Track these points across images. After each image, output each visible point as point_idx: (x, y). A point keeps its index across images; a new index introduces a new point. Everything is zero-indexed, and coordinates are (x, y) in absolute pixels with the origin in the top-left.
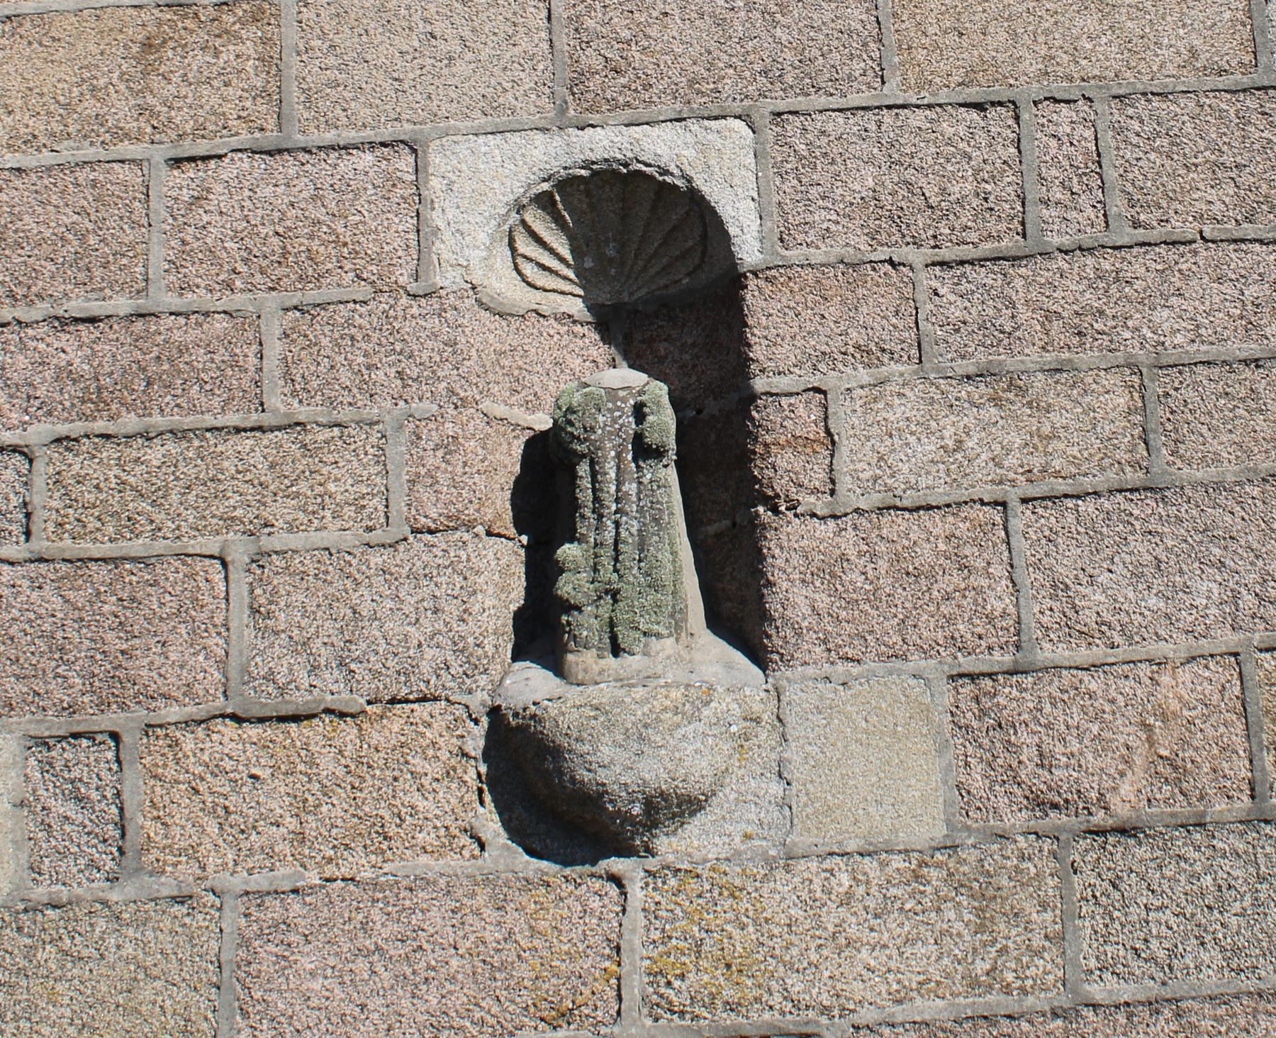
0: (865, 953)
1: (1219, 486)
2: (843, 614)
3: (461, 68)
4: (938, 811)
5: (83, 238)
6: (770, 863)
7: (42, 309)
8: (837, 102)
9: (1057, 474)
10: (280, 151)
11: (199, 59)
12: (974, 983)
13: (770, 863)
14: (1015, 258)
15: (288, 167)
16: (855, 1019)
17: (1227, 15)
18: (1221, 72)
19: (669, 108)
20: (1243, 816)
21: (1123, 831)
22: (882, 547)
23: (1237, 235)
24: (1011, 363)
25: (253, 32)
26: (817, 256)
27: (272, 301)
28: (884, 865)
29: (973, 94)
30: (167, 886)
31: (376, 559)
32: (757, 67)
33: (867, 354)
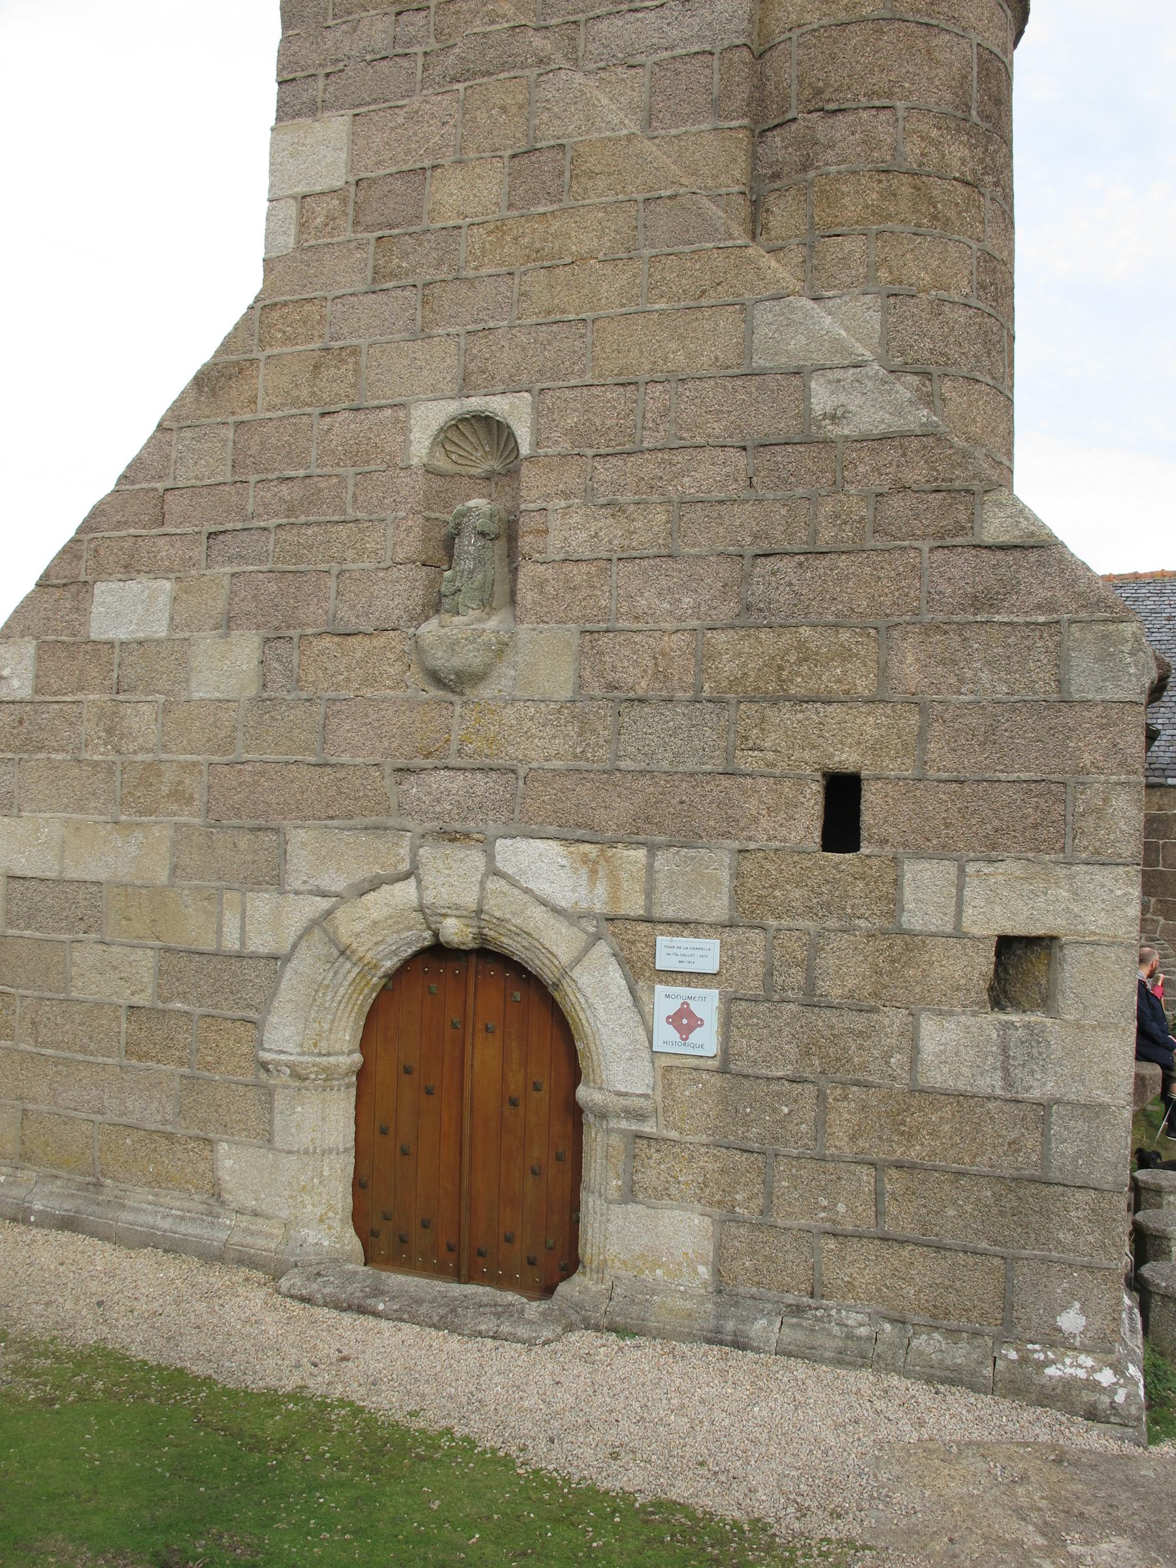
0: (536, 740)
1: (698, 557)
2: (544, 604)
3: (425, 373)
4: (570, 686)
5: (290, 446)
6: (506, 701)
7: (277, 474)
8: (565, 384)
9: (633, 548)
10: (359, 409)
11: (333, 371)
12: (575, 756)
13: (506, 701)
14: (628, 453)
15: (361, 416)
16: (530, 765)
17: (735, 340)
18: (728, 367)
19: (501, 388)
20: (688, 699)
21: (640, 700)
22: (562, 577)
23: (723, 444)
24: (621, 499)
25: (353, 360)
26: (550, 451)
27: (352, 470)
28: (547, 706)
29: (622, 379)
30: (304, 695)
31: (381, 574)
32: (537, 369)
33: (566, 495)
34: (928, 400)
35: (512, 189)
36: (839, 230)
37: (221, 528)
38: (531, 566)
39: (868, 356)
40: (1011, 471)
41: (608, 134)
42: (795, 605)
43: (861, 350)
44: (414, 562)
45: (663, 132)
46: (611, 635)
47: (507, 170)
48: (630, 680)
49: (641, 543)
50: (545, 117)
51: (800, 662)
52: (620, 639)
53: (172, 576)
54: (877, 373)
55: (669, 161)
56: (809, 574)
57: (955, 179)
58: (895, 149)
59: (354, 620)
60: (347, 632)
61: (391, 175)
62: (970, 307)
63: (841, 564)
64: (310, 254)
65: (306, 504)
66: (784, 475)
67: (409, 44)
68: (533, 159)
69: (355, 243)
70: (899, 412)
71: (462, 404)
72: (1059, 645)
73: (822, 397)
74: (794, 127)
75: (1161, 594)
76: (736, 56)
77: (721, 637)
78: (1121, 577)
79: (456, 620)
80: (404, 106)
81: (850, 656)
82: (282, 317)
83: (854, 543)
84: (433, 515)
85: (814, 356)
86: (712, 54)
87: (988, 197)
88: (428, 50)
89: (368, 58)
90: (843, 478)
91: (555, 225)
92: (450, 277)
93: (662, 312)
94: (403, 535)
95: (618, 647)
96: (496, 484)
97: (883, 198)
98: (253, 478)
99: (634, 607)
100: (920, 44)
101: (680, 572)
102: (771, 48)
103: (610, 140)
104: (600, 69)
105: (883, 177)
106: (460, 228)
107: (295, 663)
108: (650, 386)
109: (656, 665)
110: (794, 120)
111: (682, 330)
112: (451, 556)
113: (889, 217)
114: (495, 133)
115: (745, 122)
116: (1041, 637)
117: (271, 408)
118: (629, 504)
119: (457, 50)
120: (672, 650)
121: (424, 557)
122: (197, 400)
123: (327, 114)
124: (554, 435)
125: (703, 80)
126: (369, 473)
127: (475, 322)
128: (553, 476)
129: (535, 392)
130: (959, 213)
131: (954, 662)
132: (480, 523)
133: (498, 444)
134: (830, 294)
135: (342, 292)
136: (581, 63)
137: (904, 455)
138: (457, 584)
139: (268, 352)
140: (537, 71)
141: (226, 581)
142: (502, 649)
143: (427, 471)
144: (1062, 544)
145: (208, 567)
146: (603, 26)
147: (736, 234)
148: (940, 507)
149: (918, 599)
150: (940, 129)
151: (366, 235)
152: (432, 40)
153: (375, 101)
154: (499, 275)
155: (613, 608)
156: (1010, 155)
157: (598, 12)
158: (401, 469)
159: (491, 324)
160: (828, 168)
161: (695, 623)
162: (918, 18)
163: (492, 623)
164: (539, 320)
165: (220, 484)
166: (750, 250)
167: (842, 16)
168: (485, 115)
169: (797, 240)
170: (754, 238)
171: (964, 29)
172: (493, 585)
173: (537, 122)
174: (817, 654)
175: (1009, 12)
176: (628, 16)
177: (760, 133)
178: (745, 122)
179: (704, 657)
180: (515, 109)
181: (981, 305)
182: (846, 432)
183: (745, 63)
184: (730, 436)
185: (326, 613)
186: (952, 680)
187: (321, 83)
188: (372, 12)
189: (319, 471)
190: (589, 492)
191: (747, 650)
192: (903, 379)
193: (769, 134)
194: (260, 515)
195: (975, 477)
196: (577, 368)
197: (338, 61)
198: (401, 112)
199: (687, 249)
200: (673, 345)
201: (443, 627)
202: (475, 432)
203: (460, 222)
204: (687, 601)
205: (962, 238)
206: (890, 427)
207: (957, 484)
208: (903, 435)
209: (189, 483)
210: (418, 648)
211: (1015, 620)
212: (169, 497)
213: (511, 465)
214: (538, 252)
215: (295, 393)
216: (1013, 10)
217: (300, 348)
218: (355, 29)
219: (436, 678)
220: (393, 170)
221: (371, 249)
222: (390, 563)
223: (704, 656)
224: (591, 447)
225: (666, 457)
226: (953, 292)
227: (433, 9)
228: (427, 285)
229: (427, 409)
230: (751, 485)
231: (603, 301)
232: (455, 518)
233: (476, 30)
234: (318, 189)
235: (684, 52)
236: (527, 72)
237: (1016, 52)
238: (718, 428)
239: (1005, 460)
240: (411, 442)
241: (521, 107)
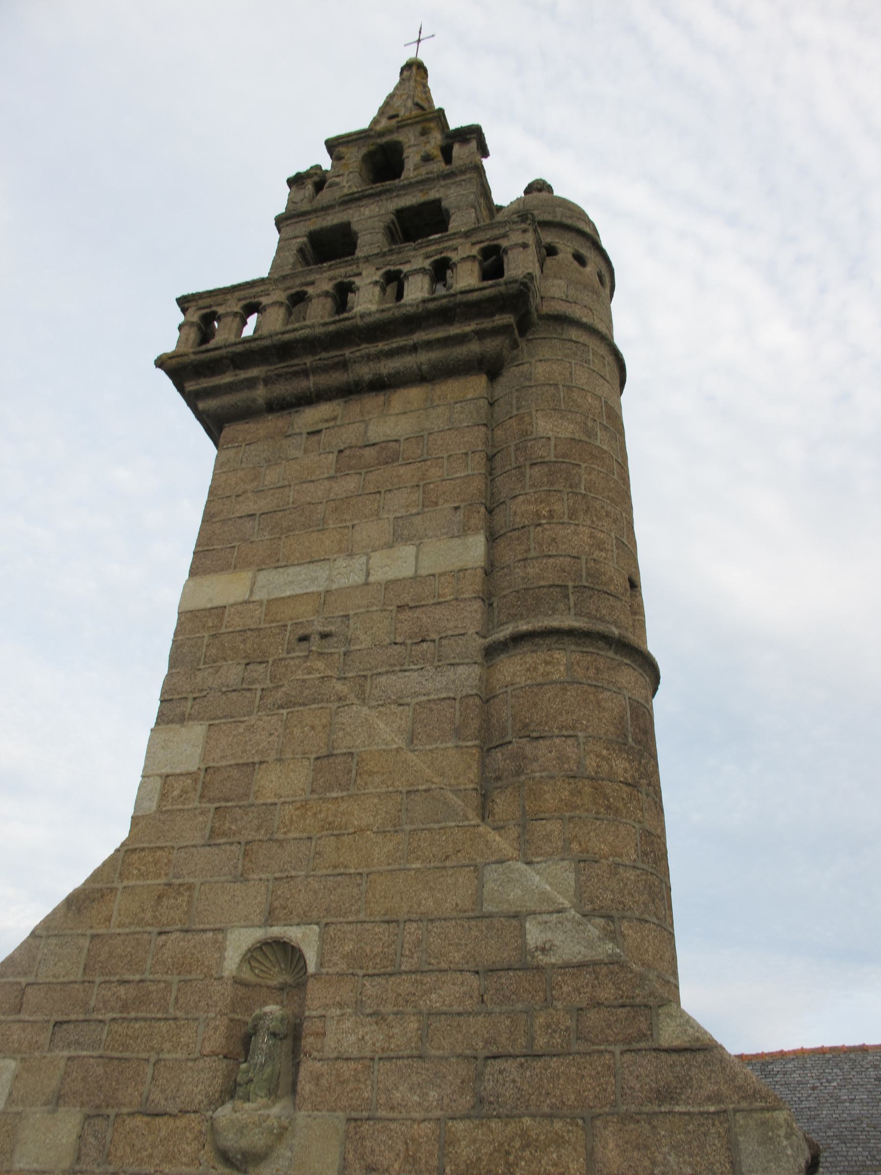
1: (442, 1058)
3: (241, 906)
5: (131, 956)
7: (118, 977)
8: (345, 920)
11: (172, 901)
15: (189, 936)
18: (465, 911)
19: (296, 920)
25: (187, 894)
26: (331, 971)
29: (387, 918)
31: (190, 1064)
33: (340, 1005)
34: (613, 936)
35: (314, 780)
36: (542, 815)
37: (65, 1018)
38: (310, 1062)
39: (567, 904)
40: (677, 987)
41: (383, 747)
42: (518, 1099)
43: (561, 900)
44: (217, 1055)
45: (421, 748)
46: (372, 1123)
47: (312, 767)
48: (386, 1163)
49: (397, 1046)
50: (341, 734)
51: (523, 1148)
52: (379, 1126)
53: (19, 1056)
54: (574, 917)
55: (424, 766)
56: (528, 1073)
57: (621, 782)
58: (579, 762)
59: (163, 1102)
60: (156, 1112)
61: (231, 766)
62: (638, 868)
63: (553, 1065)
64: (166, 815)
65: (137, 1003)
66: (508, 993)
67: (253, 683)
68: (331, 761)
69: (199, 811)
70: (591, 945)
71: (266, 932)
72: (728, 1130)
73: (534, 935)
74: (510, 747)
75: (803, 1068)
76: (471, 701)
77: (460, 1126)
78: (771, 1055)
79: (248, 1106)
80: (244, 721)
81: (563, 1142)
82: (139, 858)
83: (562, 1047)
84: (236, 1017)
85: (528, 904)
86: (454, 699)
87: (644, 793)
88: (265, 687)
89: (224, 689)
90: (552, 996)
91: (343, 806)
92: (266, 838)
93: (417, 870)
94: (211, 1032)
95: (376, 1133)
96: (288, 994)
97: (572, 794)
98: (98, 980)
99: (390, 1098)
100: (592, 697)
101: (428, 1070)
102: (494, 697)
103: (384, 751)
104: (379, 705)
105: (571, 780)
106: (276, 804)
107: (108, 1138)
108: (408, 925)
109: (407, 1150)
110: (510, 742)
111: (432, 883)
112: (247, 1051)
113: (577, 807)
114: (306, 742)
115: (477, 742)
116: (713, 1124)
117: (121, 925)
118: (389, 1014)
119: (284, 689)
120: (420, 1136)
121: (226, 1051)
122: (66, 916)
123: (190, 723)
124: (335, 958)
125: (448, 715)
126: (191, 981)
127: (281, 871)
128: (332, 990)
129: (322, 924)
130: (625, 805)
131: (647, 1147)
132: (274, 1025)
133: (291, 962)
134: (538, 859)
135: (185, 844)
136: (366, 701)
137: (597, 978)
138: (251, 1075)
139: (125, 883)
140: (337, 704)
141: (62, 1064)
142: (282, 1133)
143: (235, 982)
144: (721, 1046)
145: (50, 1050)
146: (383, 679)
147: (471, 817)
148: (626, 1019)
149: (614, 1093)
150: (608, 749)
151: (208, 805)
152: (268, 682)
153: (225, 717)
154: (301, 839)
155: (374, 1100)
156: (656, 765)
157: (380, 670)
158: (215, 979)
159: (293, 873)
160: (533, 774)
161: (438, 1113)
162: (589, 682)
163: (276, 1110)
164: (328, 872)
165: (72, 982)
166: (481, 828)
167: (540, 680)
168: (300, 731)
169: (514, 822)
170: (483, 819)
171: (619, 689)
172: (279, 1076)
173: (335, 737)
174: (537, 1140)
175: (647, 679)
176: (400, 674)
177: (486, 750)
178: (477, 742)
179: (446, 1143)
180: (320, 728)
181: (645, 867)
182: (553, 961)
183: (477, 706)
184: (467, 963)
185: (141, 1095)
186: (647, 1163)
187: (190, 703)
188: (230, 662)
189: (151, 977)
190: (359, 1004)
191: (480, 1137)
192: (592, 921)
193: (493, 750)
194: (99, 1010)
195: (651, 994)
196: (354, 908)
197: (202, 690)
198: (243, 725)
199: (436, 826)
200: (425, 894)
201: (235, 1112)
202: (275, 952)
203: (276, 800)
204: (433, 1094)
205: (628, 821)
206: (585, 956)
207: (638, 1000)
208: (595, 963)
209: (47, 980)
210: (213, 1130)
211: (692, 1110)
212: (29, 990)
213: (300, 980)
214: (330, 824)
215: (141, 915)
216: (650, 677)
217: (149, 882)
218: (217, 672)
219: (225, 1157)
220: (233, 762)
221: (211, 815)
222: (197, 1055)
223: (446, 1142)
224: (362, 968)
225: (418, 978)
226: (625, 858)
227: (270, 663)
228: (248, 843)
229: (240, 933)
230: (483, 1001)
231: (375, 860)
232: (254, 1020)
233: (298, 677)
234: (178, 771)
235: (436, 697)
236: (330, 705)
237: (654, 700)
238: (457, 956)
239: (672, 980)
240: (225, 958)
241: (324, 727)
